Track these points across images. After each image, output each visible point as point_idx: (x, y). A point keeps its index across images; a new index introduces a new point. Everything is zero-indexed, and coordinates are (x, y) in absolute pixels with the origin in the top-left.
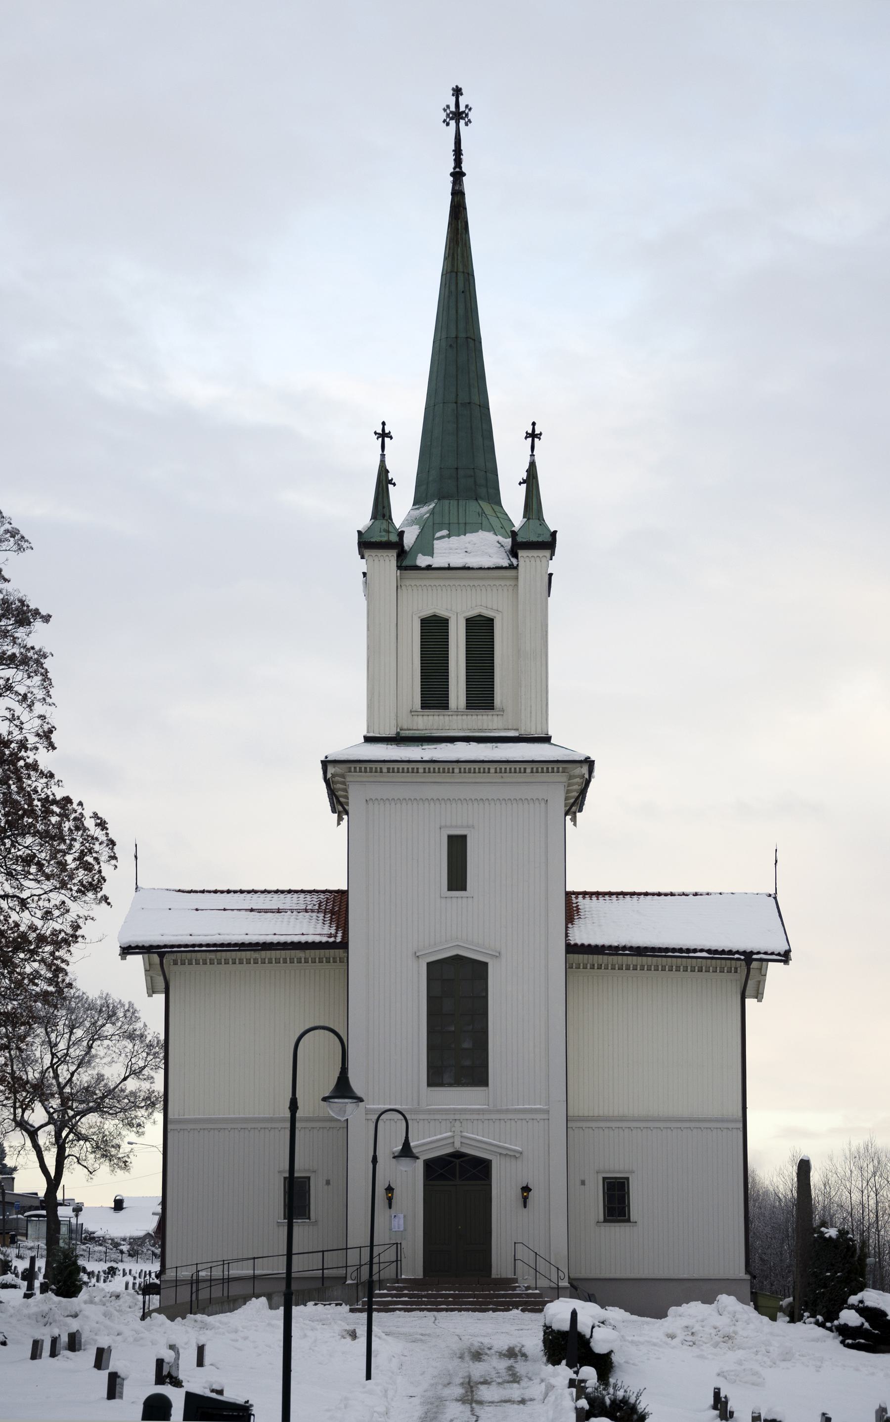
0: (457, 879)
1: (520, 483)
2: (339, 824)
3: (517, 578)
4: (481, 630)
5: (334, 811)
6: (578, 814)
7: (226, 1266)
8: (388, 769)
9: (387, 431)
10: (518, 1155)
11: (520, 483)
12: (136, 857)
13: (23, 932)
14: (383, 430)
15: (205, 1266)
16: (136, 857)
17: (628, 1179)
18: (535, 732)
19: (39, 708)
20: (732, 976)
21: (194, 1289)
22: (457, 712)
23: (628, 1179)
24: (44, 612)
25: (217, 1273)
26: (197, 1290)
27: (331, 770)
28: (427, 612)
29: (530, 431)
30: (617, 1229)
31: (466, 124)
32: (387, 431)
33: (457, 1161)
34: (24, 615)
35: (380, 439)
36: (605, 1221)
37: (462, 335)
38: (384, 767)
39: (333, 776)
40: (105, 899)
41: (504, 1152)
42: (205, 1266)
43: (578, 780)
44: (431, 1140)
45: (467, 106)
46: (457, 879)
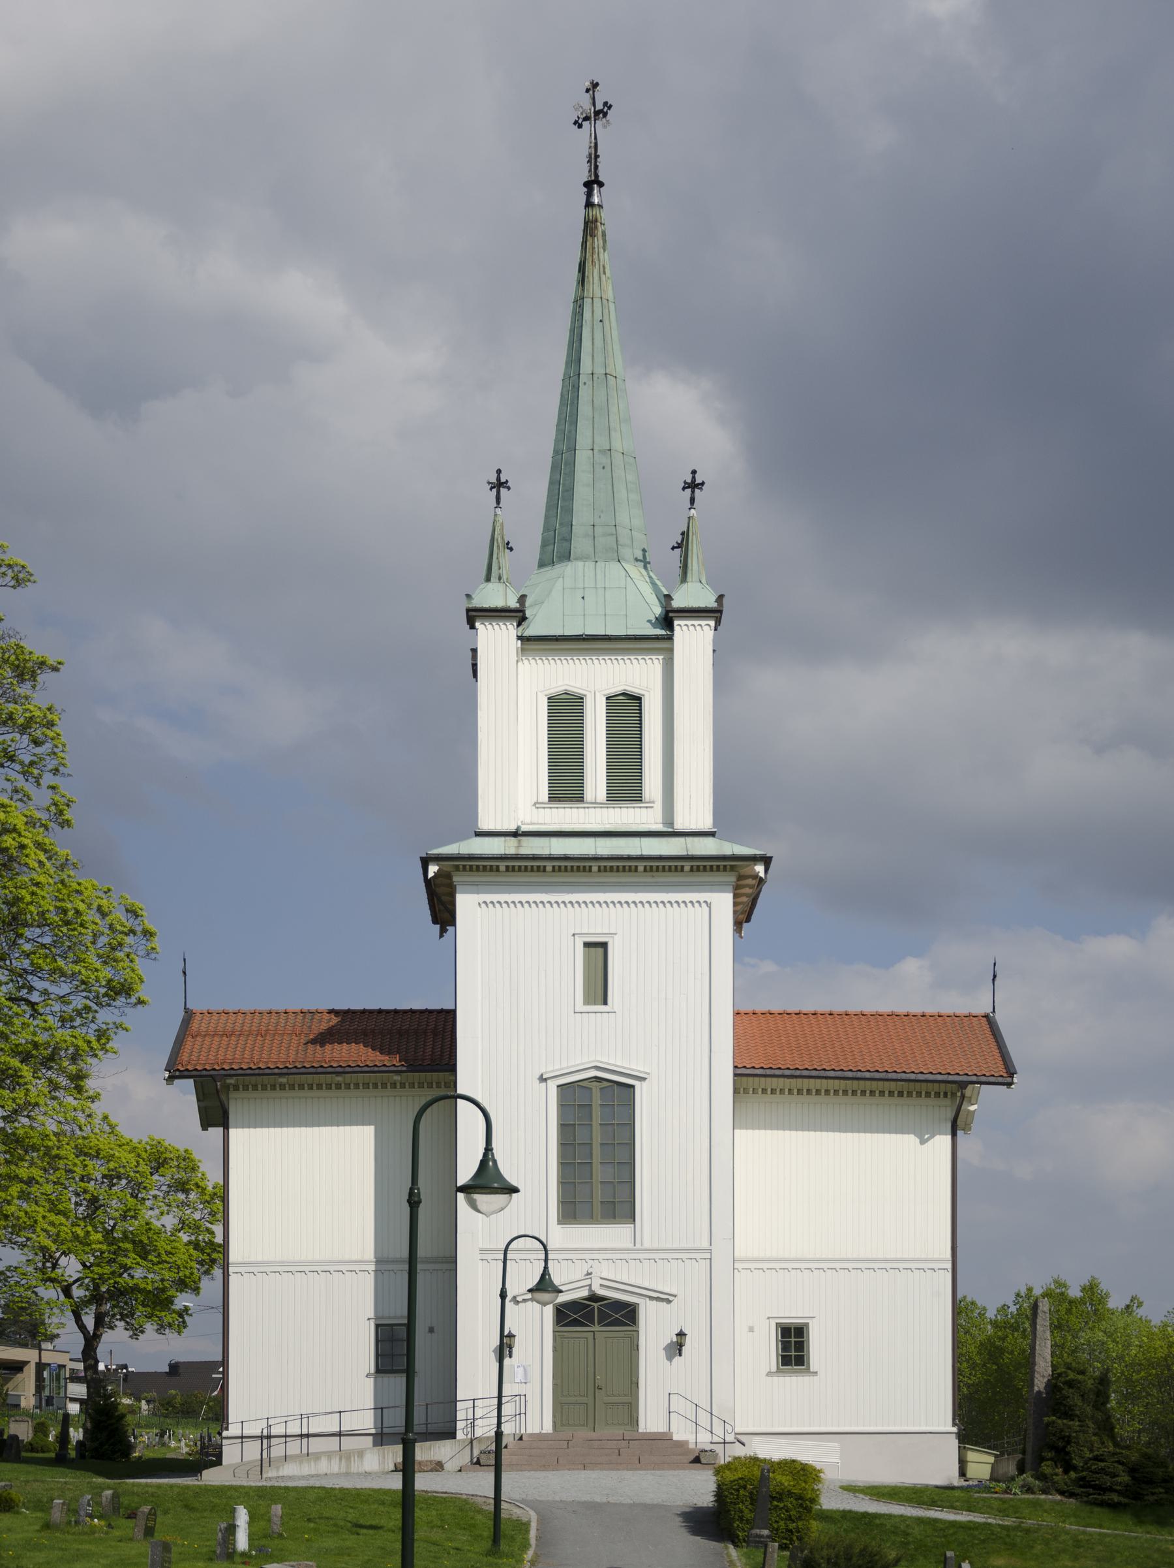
0: (598, 990)
1: (673, 548)
2: (441, 936)
3: (671, 650)
4: (626, 708)
5: (435, 922)
6: (745, 925)
7: (305, 1421)
8: (507, 867)
9: (503, 480)
10: (671, 1298)
11: (673, 548)
12: (184, 973)
13: (170, 1300)
14: (498, 479)
15: (278, 1420)
16: (184, 973)
17: (807, 1324)
18: (592, 950)
19: (48, 779)
20: (948, 1102)
21: (265, 1446)
22: (596, 804)
23: (807, 1324)
24: (51, 661)
25: (294, 1429)
26: (269, 1447)
27: (433, 869)
28: (557, 688)
29: (689, 481)
30: (788, 1378)
31: (605, 127)
32: (503, 480)
33: (596, 1305)
34: (27, 670)
35: (494, 490)
36: (778, 1370)
37: (600, 371)
38: (502, 865)
39: (436, 875)
40: (140, 1002)
41: (655, 1295)
42: (278, 1420)
43: (750, 881)
44: (572, 1283)
45: (605, 104)
46: (598, 990)
